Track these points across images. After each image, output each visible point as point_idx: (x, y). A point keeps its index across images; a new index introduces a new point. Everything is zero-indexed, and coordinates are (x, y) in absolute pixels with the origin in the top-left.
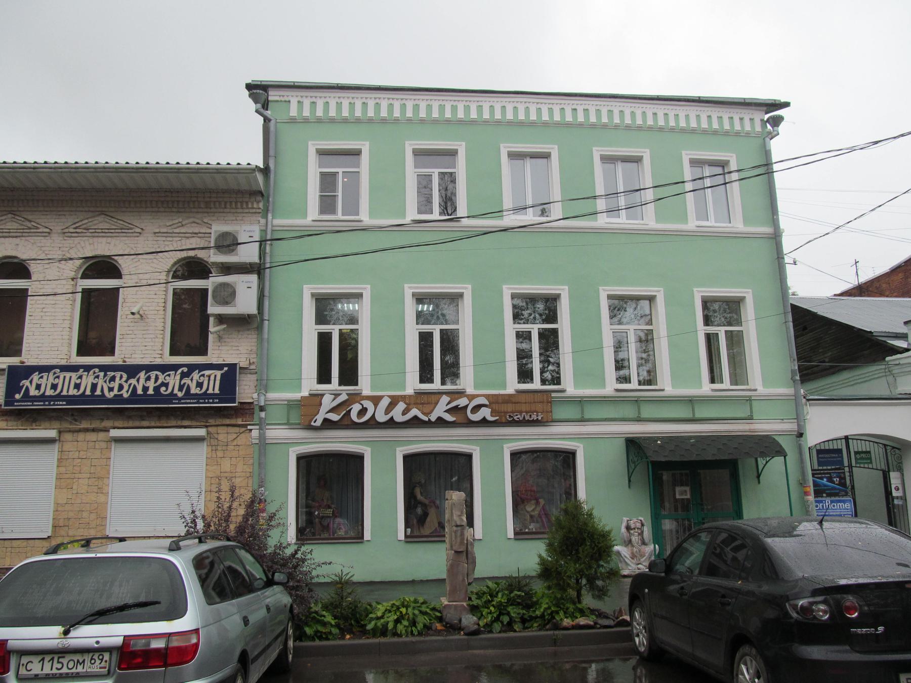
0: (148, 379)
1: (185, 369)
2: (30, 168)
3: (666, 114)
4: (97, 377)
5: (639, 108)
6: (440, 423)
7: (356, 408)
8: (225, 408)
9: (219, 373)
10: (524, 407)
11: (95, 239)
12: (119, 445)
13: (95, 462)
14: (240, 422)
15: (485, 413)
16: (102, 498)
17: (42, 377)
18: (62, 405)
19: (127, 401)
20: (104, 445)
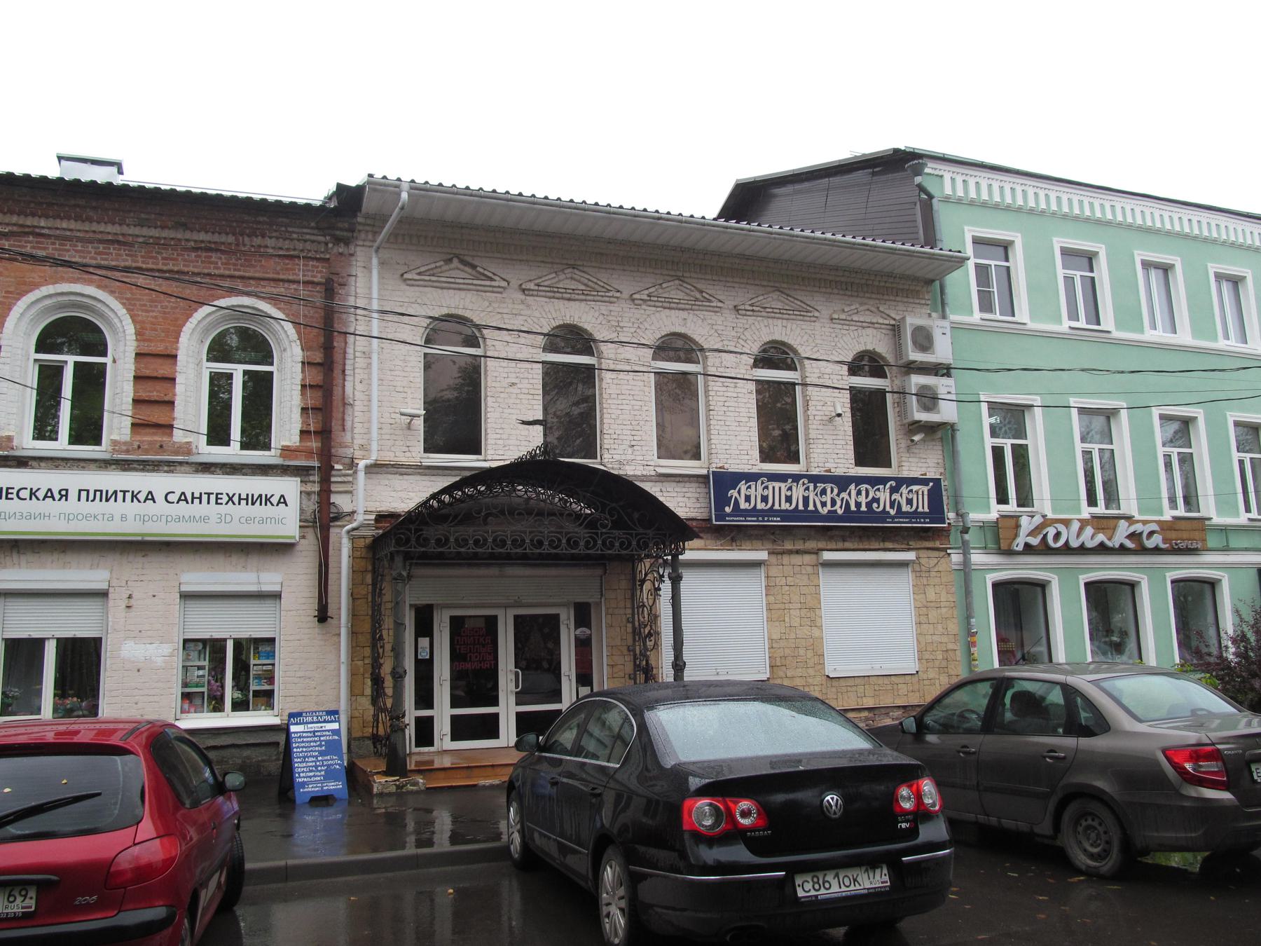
0: (859, 493)
1: (893, 483)
2: (626, 215)
3: (1112, 206)
4: (807, 489)
5: (1222, 220)
6: (1122, 550)
7: (1051, 532)
8: (923, 529)
9: (926, 489)
10: (1185, 535)
11: (770, 321)
12: (827, 570)
13: (805, 590)
14: (937, 544)
15: (1156, 540)
16: (816, 632)
17: (749, 487)
18: (776, 522)
19: (840, 518)
20: (809, 569)
